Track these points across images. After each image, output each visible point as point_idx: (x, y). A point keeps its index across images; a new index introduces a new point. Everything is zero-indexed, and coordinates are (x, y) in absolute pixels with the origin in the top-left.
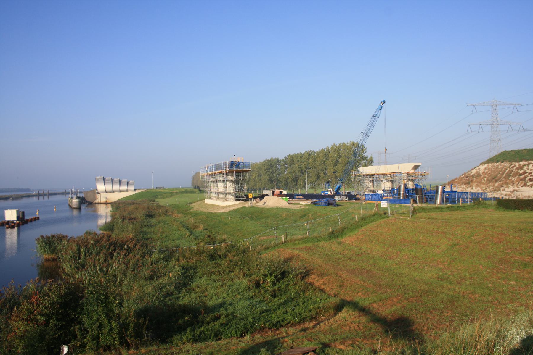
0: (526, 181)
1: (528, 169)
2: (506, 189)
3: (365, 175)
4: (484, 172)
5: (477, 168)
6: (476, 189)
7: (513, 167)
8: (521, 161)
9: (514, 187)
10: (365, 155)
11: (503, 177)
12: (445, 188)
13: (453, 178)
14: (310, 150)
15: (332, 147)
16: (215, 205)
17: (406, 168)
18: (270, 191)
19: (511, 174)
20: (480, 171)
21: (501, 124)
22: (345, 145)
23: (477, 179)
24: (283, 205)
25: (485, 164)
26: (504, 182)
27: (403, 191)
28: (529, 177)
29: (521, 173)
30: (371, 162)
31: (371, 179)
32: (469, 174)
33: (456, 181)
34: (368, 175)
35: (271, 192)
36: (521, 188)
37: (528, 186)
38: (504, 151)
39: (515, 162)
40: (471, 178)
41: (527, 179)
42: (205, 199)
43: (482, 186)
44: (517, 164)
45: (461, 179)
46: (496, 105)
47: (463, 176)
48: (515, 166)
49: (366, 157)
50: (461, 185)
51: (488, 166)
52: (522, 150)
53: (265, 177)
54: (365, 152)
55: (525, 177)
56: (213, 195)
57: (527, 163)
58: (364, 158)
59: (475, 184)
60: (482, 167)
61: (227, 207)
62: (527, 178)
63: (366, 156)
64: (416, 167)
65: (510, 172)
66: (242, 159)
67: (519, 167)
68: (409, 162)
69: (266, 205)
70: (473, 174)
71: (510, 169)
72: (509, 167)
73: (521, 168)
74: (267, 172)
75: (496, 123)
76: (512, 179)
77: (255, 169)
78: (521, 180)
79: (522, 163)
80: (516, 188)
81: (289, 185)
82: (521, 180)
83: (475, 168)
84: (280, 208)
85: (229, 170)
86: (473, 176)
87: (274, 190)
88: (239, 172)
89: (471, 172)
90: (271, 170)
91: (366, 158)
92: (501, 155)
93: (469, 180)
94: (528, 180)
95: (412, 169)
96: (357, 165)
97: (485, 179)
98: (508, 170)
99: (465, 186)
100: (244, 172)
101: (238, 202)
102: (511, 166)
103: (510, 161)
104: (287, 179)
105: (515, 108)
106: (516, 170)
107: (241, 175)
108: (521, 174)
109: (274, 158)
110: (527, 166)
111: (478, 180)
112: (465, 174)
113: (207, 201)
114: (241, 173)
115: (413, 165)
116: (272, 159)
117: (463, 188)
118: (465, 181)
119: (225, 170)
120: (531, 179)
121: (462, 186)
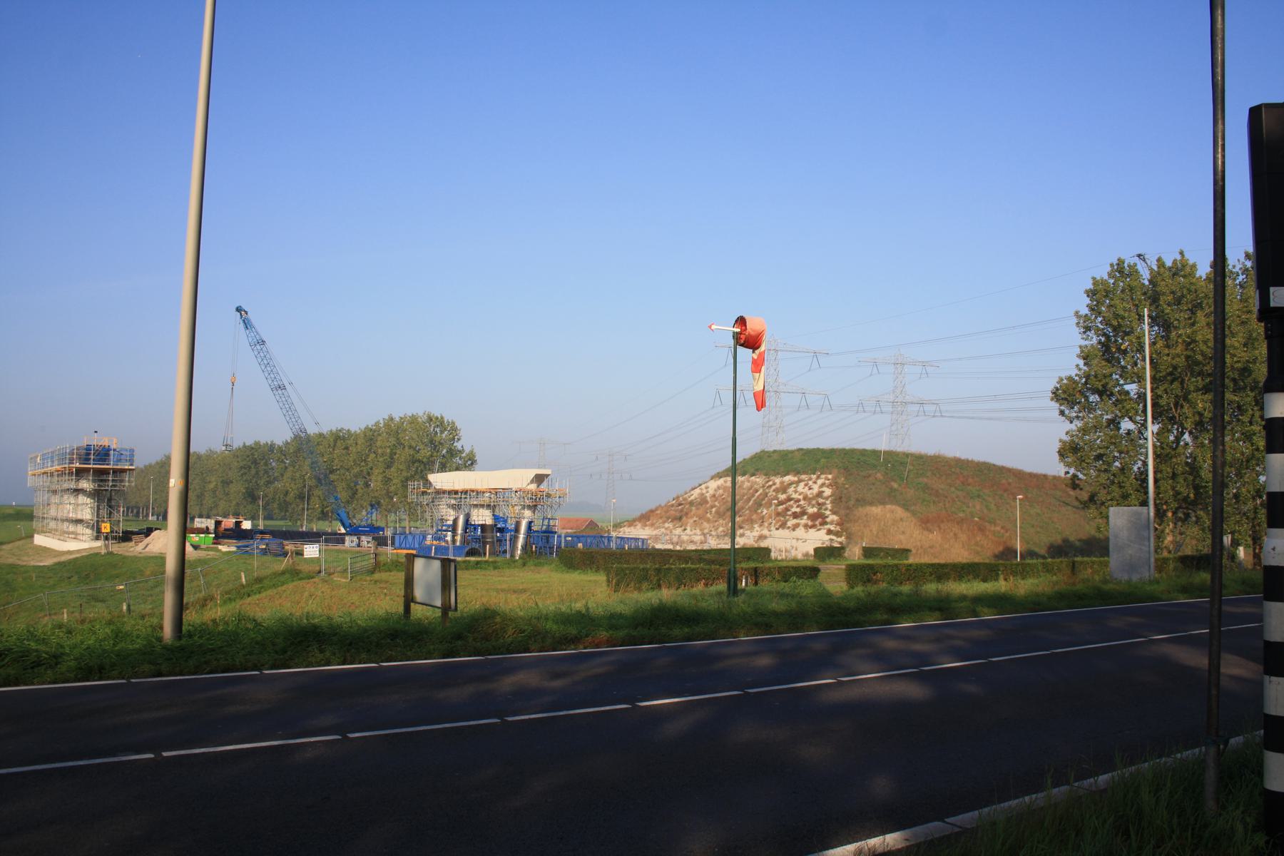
0: (787, 517)
1: (796, 492)
2: (748, 533)
3: (440, 492)
4: (714, 496)
5: (703, 486)
6: (691, 531)
7: (770, 486)
8: (787, 474)
9: (762, 530)
10: (458, 445)
11: (747, 507)
12: (533, 524)
13: (653, 507)
14: (339, 428)
15: (387, 425)
16: (49, 549)
17: (519, 478)
18: (209, 520)
19: (764, 502)
20: (707, 492)
21: (785, 392)
22: (413, 420)
23: (697, 509)
24: (838, 589)
25: (721, 477)
26: (746, 518)
27: (463, 530)
28: (794, 509)
29: (782, 501)
30: (469, 462)
31: (453, 502)
32: (685, 499)
33: (659, 512)
34: (444, 492)
35: (213, 522)
36: (775, 532)
37: (789, 528)
38: (761, 452)
39: (775, 476)
40: (687, 506)
41: (789, 513)
42: (36, 535)
43: (705, 524)
44: (778, 480)
45: (668, 507)
46: (776, 351)
47: (674, 502)
48: (774, 484)
49: (460, 451)
50: (664, 522)
51: (725, 482)
52: (792, 452)
53: (238, 488)
54: (459, 439)
55: (787, 509)
56: (52, 524)
57: (796, 479)
58: (453, 453)
59: (691, 521)
60: (713, 485)
61: (69, 552)
62: (789, 510)
63: (460, 448)
64: (539, 479)
65: (761, 497)
66: (115, 441)
67: (781, 487)
68: (526, 466)
69: (147, 550)
70: (692, 498)
71: (764, 490)
72: (763, 486)
73: (784, 489)
74: (242, 475)
75: (775, 389)
76: (762, 512)
77: (218, 466)
78: (778, 514)
79: (788, 478)
80: (765, 532)
81: (290, 510)
82: (778, 514)
83: (700, 485)
84: (153, 557)
85: (78, 465)
86: (691, 503)
87: (220, 519)
88: (105, 472)
89: (689, 494)
90: (253, 471)
91: (461, 452)
92: (754, 460)
93: (682, 511)
94: (790, 515)
95: (532, 482)
96: (421, 468)
97: (714, 510)
98: (759, 493)
99: (671, 525)
100: (115, 471)
101: (99, 544)
102: (767, 485)
103: (766, 475)
104: (287, 493)
105: (815, 359)
106: (774, 494)
107: (110, 479)
108: (781, 503)
109: (263, 442)
110: (795, 485)
111: (700, 512)
112: (678, 497)
113: (39, 540)
114: (109, 473)
115: (532, 473)
116: (257, 443)
117: (666, 529)
118: (674, 512)
119: (67, 466)
120: (796, 512)
121: (667, 525)
